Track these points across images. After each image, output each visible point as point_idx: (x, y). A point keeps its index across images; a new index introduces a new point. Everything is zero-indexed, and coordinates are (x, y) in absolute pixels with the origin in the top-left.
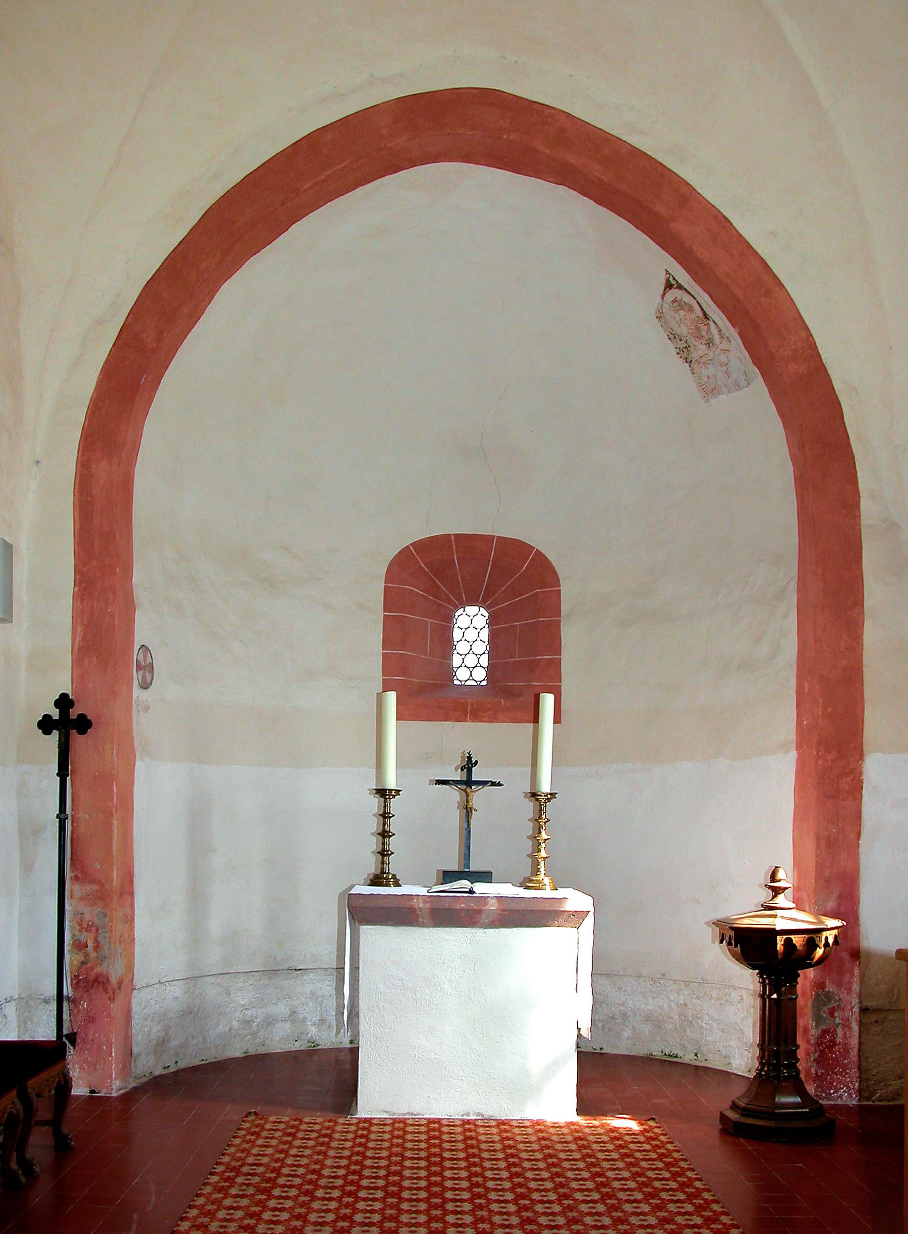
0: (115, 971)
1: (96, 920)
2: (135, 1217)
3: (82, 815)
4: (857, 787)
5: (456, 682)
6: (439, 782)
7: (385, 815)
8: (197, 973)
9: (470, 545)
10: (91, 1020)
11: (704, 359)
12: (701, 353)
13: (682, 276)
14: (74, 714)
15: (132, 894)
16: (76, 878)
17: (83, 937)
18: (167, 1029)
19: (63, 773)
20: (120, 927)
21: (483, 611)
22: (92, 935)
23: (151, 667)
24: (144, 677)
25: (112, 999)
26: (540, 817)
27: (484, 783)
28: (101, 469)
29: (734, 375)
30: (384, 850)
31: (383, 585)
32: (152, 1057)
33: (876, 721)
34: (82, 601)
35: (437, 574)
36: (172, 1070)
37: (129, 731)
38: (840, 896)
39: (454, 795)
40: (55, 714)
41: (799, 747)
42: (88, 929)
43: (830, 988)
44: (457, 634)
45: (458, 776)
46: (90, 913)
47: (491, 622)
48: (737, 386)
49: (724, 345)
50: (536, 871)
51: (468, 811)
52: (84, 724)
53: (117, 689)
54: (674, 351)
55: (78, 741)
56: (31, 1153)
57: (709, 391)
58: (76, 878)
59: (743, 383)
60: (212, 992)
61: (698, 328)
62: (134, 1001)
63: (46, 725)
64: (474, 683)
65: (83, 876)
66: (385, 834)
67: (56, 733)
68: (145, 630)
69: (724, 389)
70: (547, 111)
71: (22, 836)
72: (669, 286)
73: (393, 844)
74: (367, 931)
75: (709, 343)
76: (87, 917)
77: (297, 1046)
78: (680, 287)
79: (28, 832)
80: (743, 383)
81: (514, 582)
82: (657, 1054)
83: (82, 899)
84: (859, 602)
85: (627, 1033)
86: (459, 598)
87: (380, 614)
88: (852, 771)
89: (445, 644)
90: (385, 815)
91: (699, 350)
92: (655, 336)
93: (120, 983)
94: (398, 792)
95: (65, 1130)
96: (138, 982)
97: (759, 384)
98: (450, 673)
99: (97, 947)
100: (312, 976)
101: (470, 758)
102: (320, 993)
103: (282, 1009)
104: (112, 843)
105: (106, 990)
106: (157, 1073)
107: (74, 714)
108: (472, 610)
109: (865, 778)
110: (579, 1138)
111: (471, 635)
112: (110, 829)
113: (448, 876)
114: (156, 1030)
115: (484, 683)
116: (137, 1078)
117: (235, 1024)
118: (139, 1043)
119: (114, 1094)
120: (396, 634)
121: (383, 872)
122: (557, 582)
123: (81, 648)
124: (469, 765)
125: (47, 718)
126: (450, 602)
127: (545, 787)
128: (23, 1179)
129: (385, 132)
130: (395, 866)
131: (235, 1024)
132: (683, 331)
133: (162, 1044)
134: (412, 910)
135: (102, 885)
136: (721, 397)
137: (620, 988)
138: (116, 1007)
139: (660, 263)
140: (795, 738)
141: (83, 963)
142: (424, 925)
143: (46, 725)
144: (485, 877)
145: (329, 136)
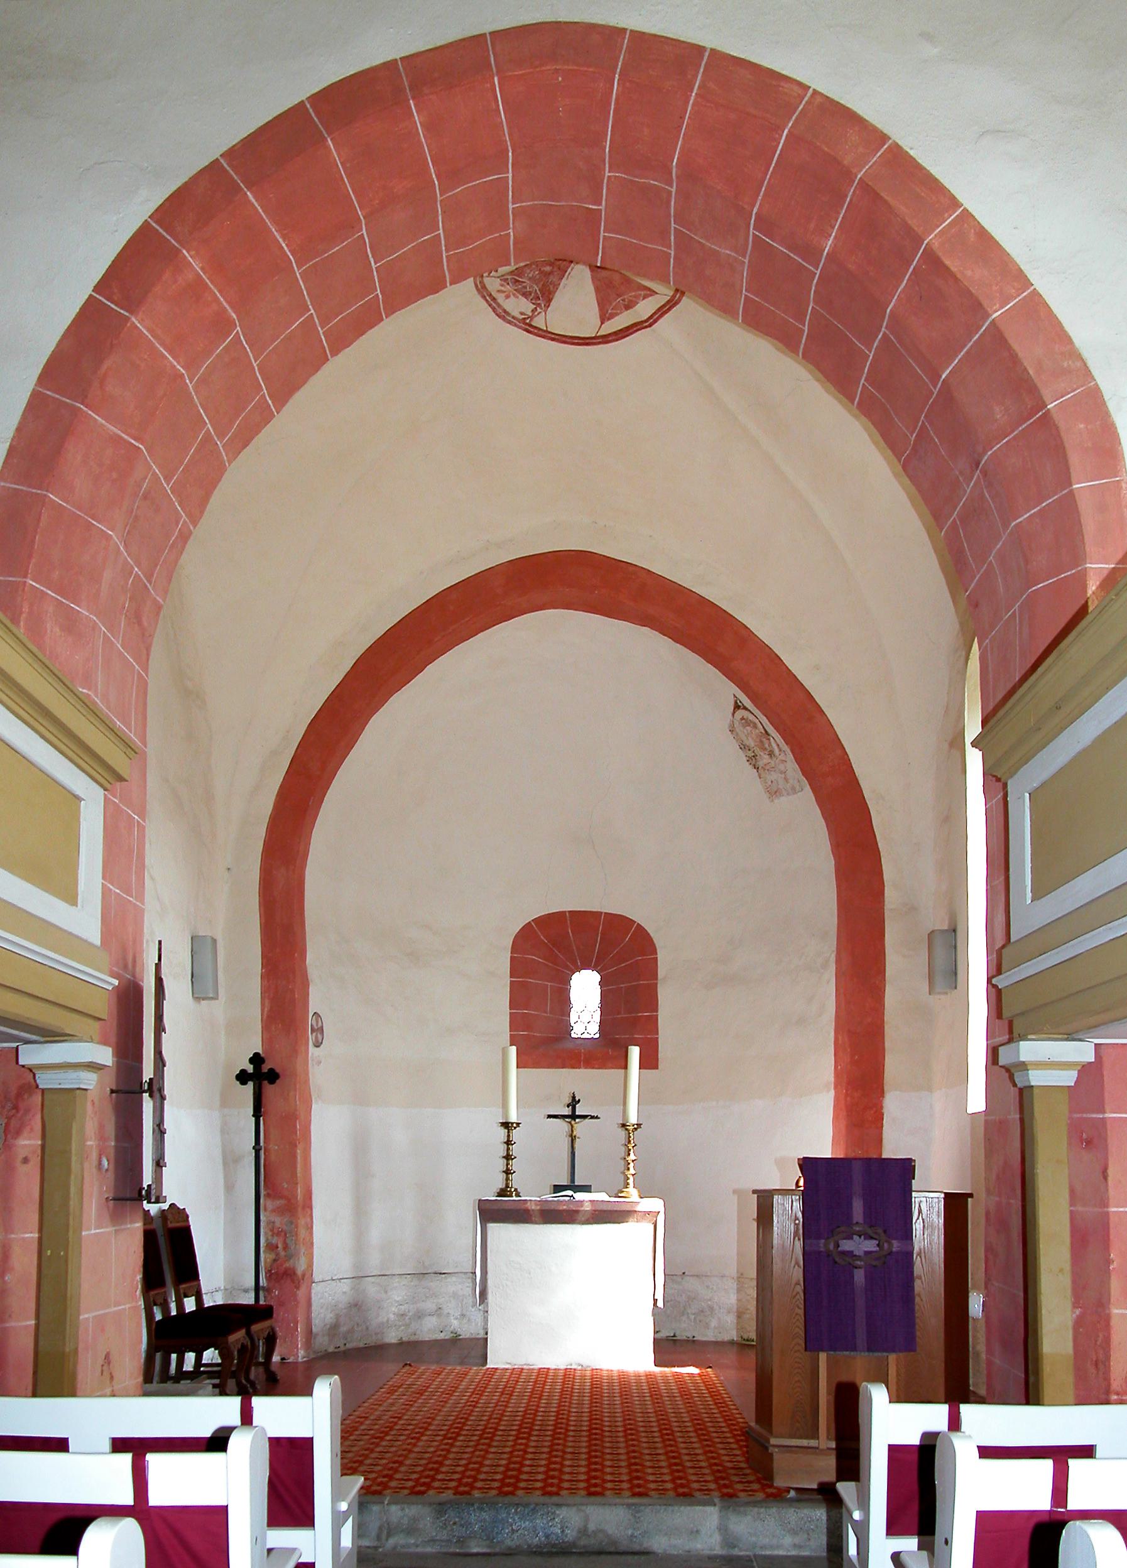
0: (301, 1267)
1: (285, 1228)
3: (273, 1147)
5: (573, 1035)
6: (550, 1116)
7: (508, 1143)
9: (582, 920)
12: (765, 761)
13: (747, 702)
14: (265, 1068)
16: (268, 1196)
18: (338, 1316)
19: (257, 1114)
20: (302, 1232)
23: (321, 1030)
24: (316, 1037)
25: (298, 1288)
26: (629, 1142)
29: (791, 781)
30: (508, 1169)
31: (509, 955)
32: (326, 1338)
35: (550, 946)
37: (307, 1081)
39: (562, 1126)
40: (250, 1069)
41: (835, 1088)
42: (278, 1234)
45: (567, 1111)
46: (278, 1221)
48: (794, 791)
49: (782, 757)
50: (627, 1185)
51: (573, 1139)
52: (273, 1076)
53: (296, 1048)
54: (745, 759)
55: (269, 1089)
56: (252, 1376)
57: (773, 793)
58: (268, 1196)
59: (798, 788)
60: (372, 1289)
61: (761, 741)
62: (313, 1291)
63: (243, 1077)
67: (251, 1084)
68: (318, 1000)
69: (784, 793)
71: (225, 1164)
72: (737, 707)
73: (515, 1165)
74: (492, 1227)
75: (771, 754)
76: (278, 1224)
77: (442, 1336)
78: (745, 708)
79: (229, 1160)
80: (798, 788)
81: (622, 951)
83: (273, 1211)
84: (882, 971)
85: (714, 1323)
86: (574, 963)
87: (508, 980)
89: (563, 1003)
90: (508, 1143)
91: (764, 759)
92: (731, 746)
93: (304, 1275)
94: (518, 1124)
96: (317, 1276)
97: (808, 794)
98: (569, 1028)
99: (286, 1247)
100: (454, 1279)
101: (574, 1097)
102: (461, 1293)
103: (430, 1305)
104: (295, 1168)
105: (293, 1281)
107: (265, 1068)
109: (885, 1111)
110: (649, 1376)
112: (294, 1156)
113: (557, 1188)
114: (329, 1317)
115: (597, 1036)
116: (315, 1352)
117: (392, 1316)
118: (317, 1324)
120: (519, 996)
121: (507, 1186)
123: (268, 1017)
124: (574, 1102)
125: (243, 1072)
126: (567, 967)
127: (633, 1119)
130: (516, 1182)
131: (392, 1316)
132: (751, 743)
133: (334, 1328)
134: (527, 1211)
135: (289, 1200)
136: (782, 798)
137: (708, 1287)
138: (301, 1293)
139: (729, 690)
140: (833, 1079)
141: (275, 1260)
142: (536, 1223)
143: (243, 1077)
144: (586, 1189)
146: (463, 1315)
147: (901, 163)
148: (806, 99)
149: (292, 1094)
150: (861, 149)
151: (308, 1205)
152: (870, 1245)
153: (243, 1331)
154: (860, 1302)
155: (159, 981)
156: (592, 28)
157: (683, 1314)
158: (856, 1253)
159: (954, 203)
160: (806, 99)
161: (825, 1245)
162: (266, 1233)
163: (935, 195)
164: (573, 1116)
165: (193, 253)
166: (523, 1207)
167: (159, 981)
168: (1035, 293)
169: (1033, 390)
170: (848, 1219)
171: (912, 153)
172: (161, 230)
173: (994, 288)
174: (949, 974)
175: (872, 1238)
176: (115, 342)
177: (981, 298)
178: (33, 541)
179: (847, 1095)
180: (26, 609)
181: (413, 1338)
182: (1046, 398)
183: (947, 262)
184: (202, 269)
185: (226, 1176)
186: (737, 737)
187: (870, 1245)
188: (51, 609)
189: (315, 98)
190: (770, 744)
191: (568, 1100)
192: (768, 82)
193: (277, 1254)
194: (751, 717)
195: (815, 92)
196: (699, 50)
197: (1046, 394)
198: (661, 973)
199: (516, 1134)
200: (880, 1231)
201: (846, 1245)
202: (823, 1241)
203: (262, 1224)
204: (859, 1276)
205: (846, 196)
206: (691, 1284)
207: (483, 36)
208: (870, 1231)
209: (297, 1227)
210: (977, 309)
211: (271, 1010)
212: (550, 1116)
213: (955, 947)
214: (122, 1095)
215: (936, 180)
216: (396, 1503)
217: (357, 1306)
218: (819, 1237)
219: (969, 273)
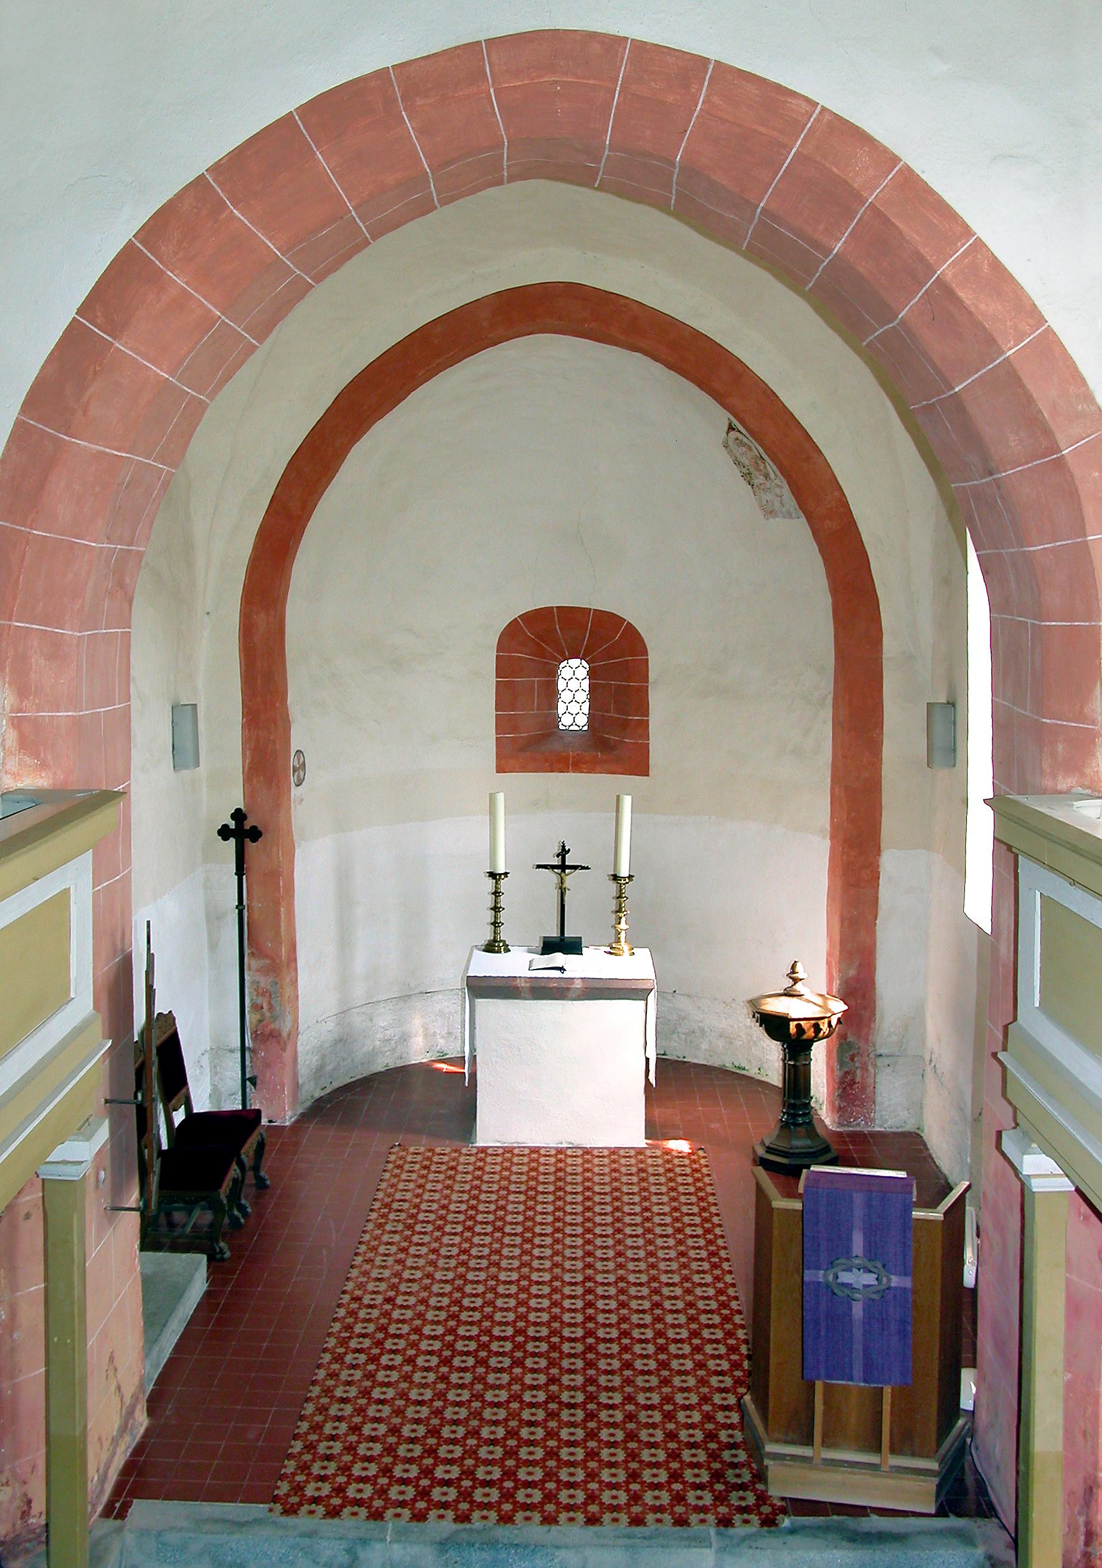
0: (286, 1027)
1: (269, 987)
2: (325, 1252)
3: (257, 905)
4: (875, 877)
5: (561, 727)
6: (539, 867)
7: (497, 893)
8: (346, 1008)
9: (570, 616)
10: (268, 1066)
11: (762, 487)
14: (247, 826)
15: (295, 960)
17: (259, 1001)
18: (323, 1057)
19: (240, 872)
20: (288, 991)
21: (584, 663)
22: (266, 999)
24: (299, 776)
25: (284, 1050)
27: (575, 867)
28: (261, 620)
31: (495, 654)
33: (890, 824)
34: (250, 730)
35: (536, 642)
36: (328, 1091)
38: (860, 965)
39: (552, 877)
40: (232, 824)
42: (263, 994)
43: (851, 1038)
44: (561, 684)
45: (556, 861)
46: (264, 982)
47: (591, 674)
49: (777, 482)
50: (618, 941)
52: (255, 834)
55: (250, 846)
57: (770, 513)
60: (358, 1021)
63: (224, 833)
64: (577, 728)
65: (259, 953)
66: (496, 909)
67: (232, 841)
70: (622, 301)
72: (731, 428)
73: (503, 916)
74: (479, 1002)
75: (767, 476)
76: (262, 985)
79: (213, 918)
82: (729, 1066)
86: (562, 654)
87: (493, 680)
88: (871, 864)
89: (551, 694)
90: (497, 893)
91: (759, 479)
94: (506, 874)
95: (262, 1173)
97: (803, 520)
98: (557, 719)
100: (440, 996)
101: (564, 847)
104: (279, 927)
106: (317, 1095)
107: (247, 826)
108: (575, 662)
109: (881, 870)
111: (574, 684)
112: (279, 914)
114: (315, 1060)
115: (586, 728)
119: (287, 1124)
120: (506, 696)
122: (645, 652)
123: (250, 768)
124: (563, 852)
125: (225, 827)
126: (555, 659)
127: (624, 872)
128: (242, 1221)
129: (485, 324)
134: (516, 988)
135: (273, 960)
137: (699, 1008)
138: (287, 1055)
139: (723, 417)
141: (260, 1021)
143: (224, 833)
145: (439, 329)
146: (449, 1033)
147: (912, 186)
148: (815, 116)
149: (275, 849)
150: (871, 172)
151: (293, 959)
152: (869, 1279)
153: (235, 1166)
154: (858, 1333)
155: (151, 958)
156: (592, 36)
157: (673, 1033)
158: (855, 1286)
159: (967, 232)
160: (815, 116)
161: (825, 1276)
162: (250, 993)
163: (947, 223)
164: (563, 867)
165: (177, 272)
166: (513, 984)
167: (151, 958)
168: (1050, 331)
169: (1047, 432)
170: (848, 1254)
171: (923, 176)
172: (145, 251)
173: (1009, 324)
174: (946, 746)
175: (871, 1272)
176: (98, 368)
177: (995, 335)
178: (17, 582)
179: (843, 853)
180: (11, 653)
181: (400, 1064)
182: (1062, 445)
183: (961, 294)
184: (187, 283)
185: (209, 934)
186: (730, 452)
187: (869, 1279)
188: (36, 643)
189: (304, 109)
190: (765, 467)
191: (558, 850)
192: (775, 96)
193: (263, 1015)
194: (745, 440)
195: (824, 109)
196: (702, 62)
197: (1061, 438)
198: (652, 676)
199: (504, 884)
200: (879, 1265)
201: (845, 1277)
202: (822, 1272)
203: (247, 984)
204: (858, 1310)
205: (857, 213)
206: (683, 1003)
207: (479, 43)
208: (869, 1265)
209: (281, 987)
210: (991, 344)
211: (251, 762)
212: (539, 867)
213: (955, 724)
214: (114, 1105)
215: (948, 207)
216: (399, 1541)
217: (343, 1041)
218: (818, 1269)
219: (983, 307)
